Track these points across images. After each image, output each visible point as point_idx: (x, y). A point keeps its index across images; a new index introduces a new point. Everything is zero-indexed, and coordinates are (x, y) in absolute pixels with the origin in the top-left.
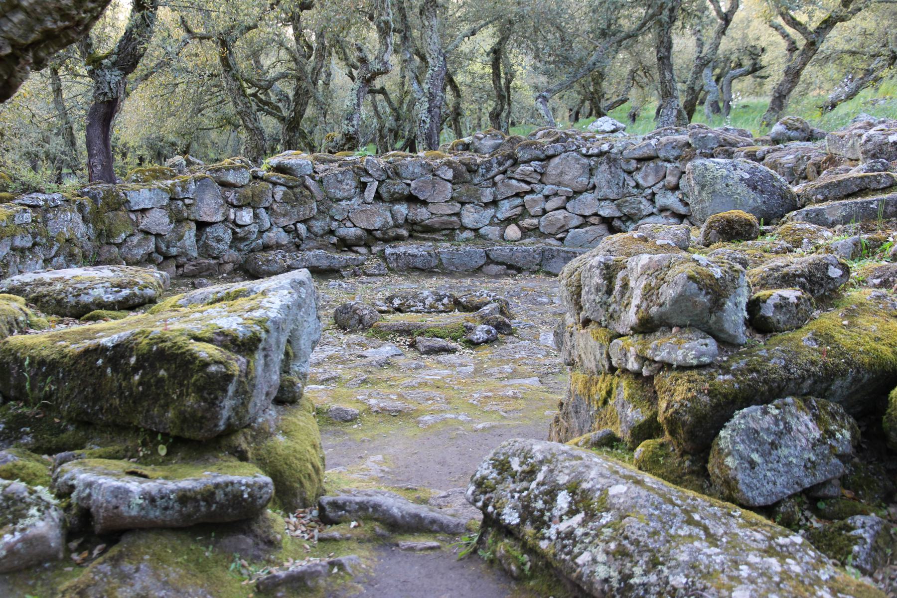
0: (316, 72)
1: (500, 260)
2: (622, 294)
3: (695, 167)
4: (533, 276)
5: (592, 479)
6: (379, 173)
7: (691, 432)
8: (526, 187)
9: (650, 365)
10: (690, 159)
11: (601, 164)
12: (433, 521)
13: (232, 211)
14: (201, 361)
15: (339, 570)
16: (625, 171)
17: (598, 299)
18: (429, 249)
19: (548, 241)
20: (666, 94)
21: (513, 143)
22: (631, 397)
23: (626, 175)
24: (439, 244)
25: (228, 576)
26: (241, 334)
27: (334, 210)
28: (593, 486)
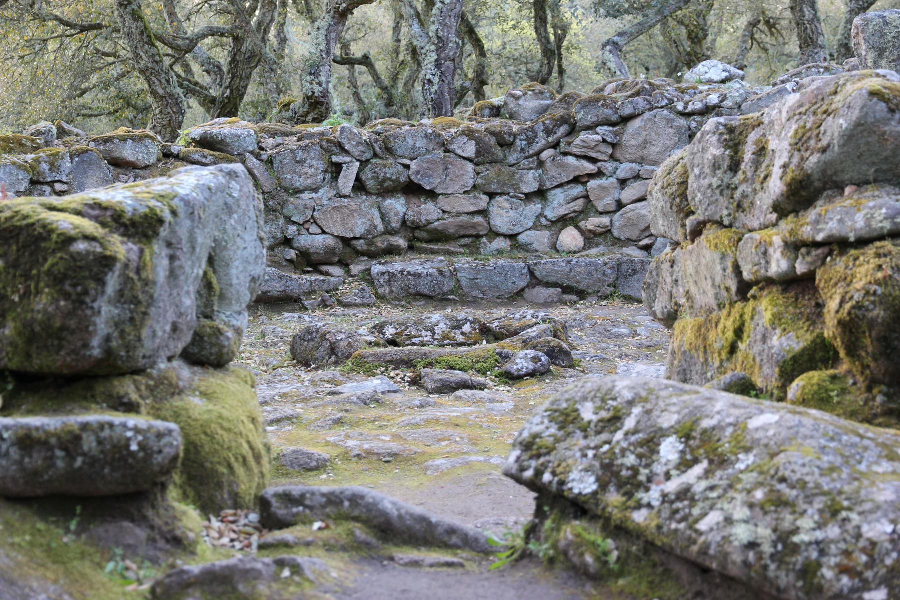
0: (263, 28)
1: (551, 280)
2: (757, 164)
3: (867, 23)
4: (604, 303)
5: (719, 413)
6: (361, 148)
7: (885, 339)
8: (590, 168)
9: (808, 254)
12: (452, 531)
14: (59, 235)
15: (293, 574)
17: (715, 182)
18: (441, 265)
19: (625, 250)
20: (806, 42)
21: (568, 104)
22: (777, 319)
24: (456, 260)
25: (101, 577)
26: (130, 209)
27: (291, 207)
28: (720, 422)
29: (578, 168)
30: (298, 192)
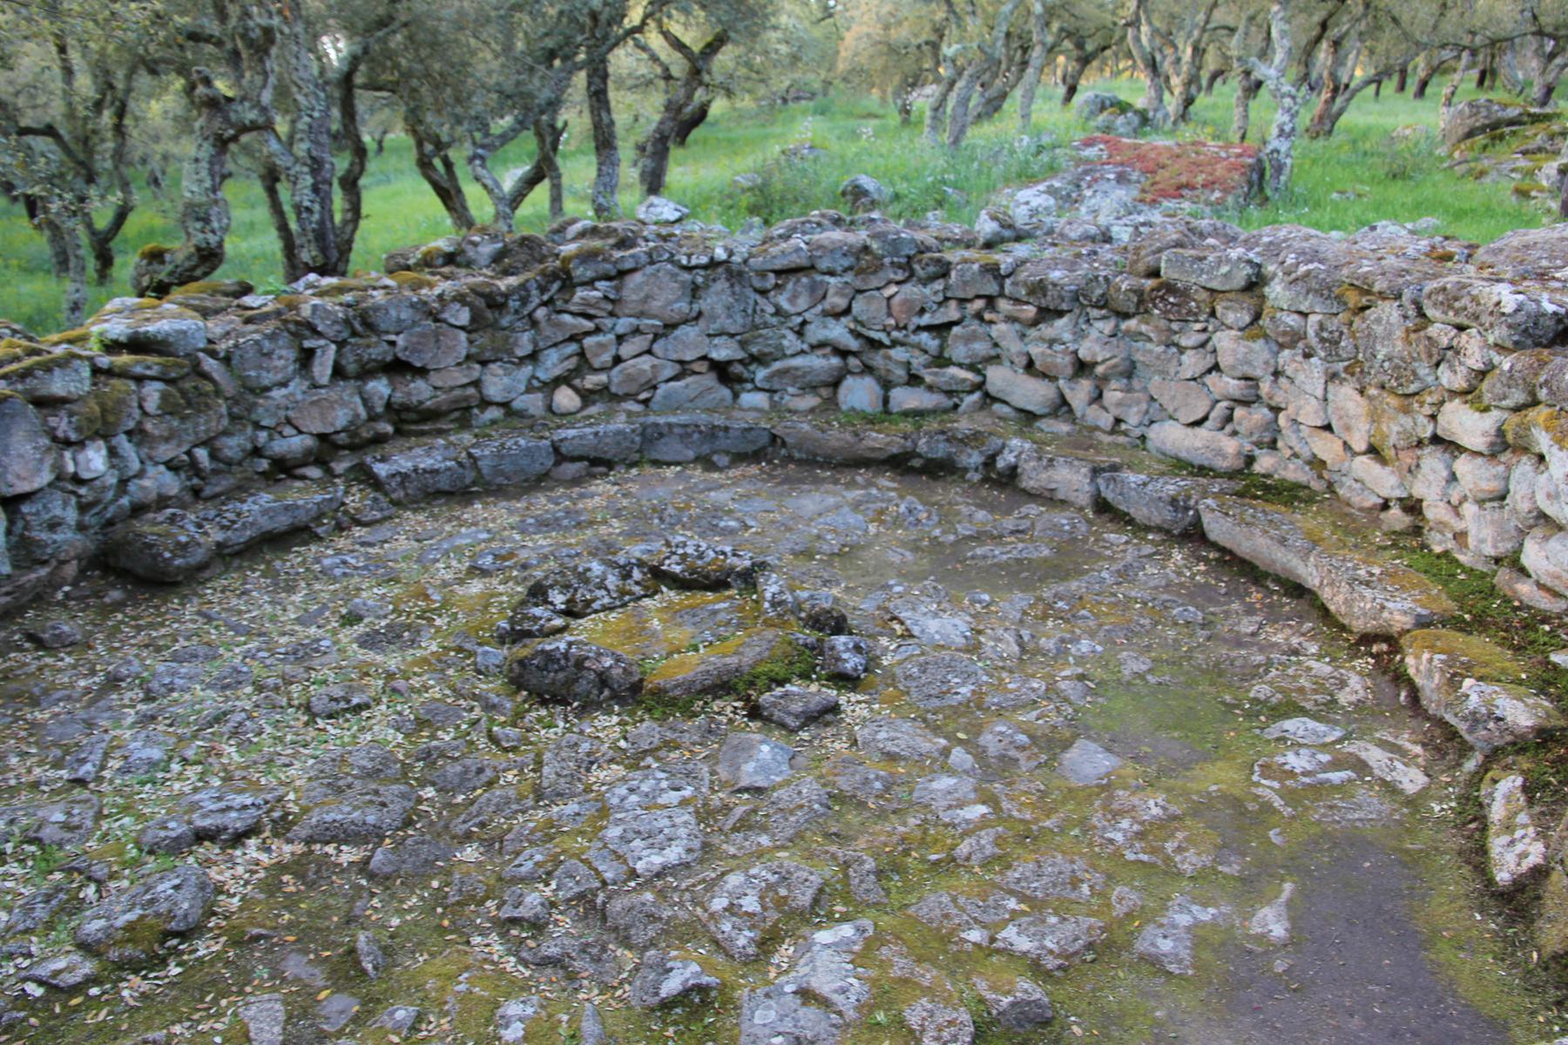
1: (576, 453)
6: (337, 327)
8: (589, 325)
10: (875, 272)
11: (714, 280)
13: (68, 455)
16: (757, 291)
23: (758, 297)
27: (260, 410)
29: (575, 326)
30: (267, 389)
